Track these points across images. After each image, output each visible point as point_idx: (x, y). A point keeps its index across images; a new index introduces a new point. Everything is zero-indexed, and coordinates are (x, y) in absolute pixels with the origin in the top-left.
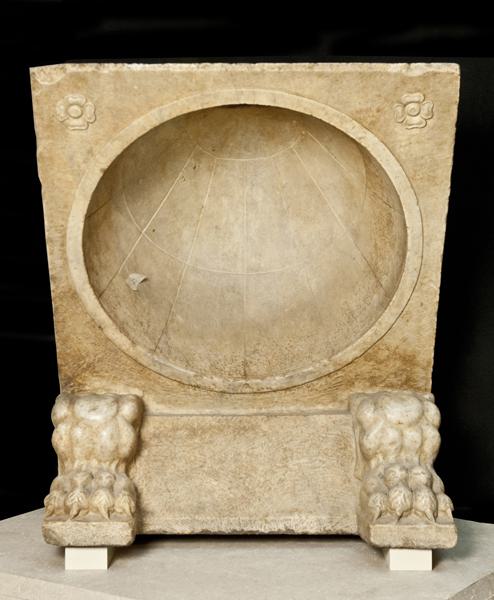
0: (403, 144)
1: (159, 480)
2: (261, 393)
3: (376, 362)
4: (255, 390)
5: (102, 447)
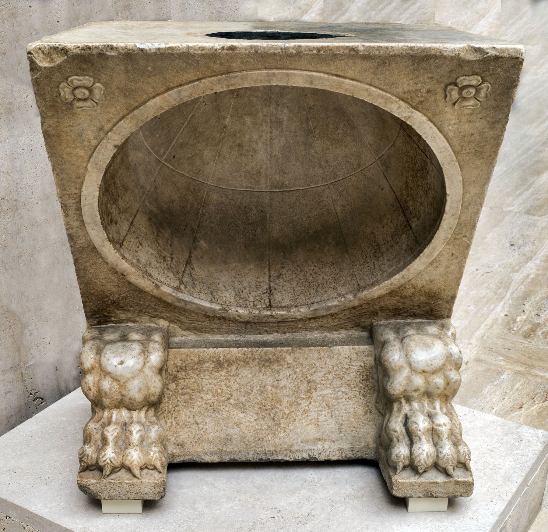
0: (452, 122)
1: (188, 413)
3: (401, 297)
4: (279, 320)
5: (130, 399)
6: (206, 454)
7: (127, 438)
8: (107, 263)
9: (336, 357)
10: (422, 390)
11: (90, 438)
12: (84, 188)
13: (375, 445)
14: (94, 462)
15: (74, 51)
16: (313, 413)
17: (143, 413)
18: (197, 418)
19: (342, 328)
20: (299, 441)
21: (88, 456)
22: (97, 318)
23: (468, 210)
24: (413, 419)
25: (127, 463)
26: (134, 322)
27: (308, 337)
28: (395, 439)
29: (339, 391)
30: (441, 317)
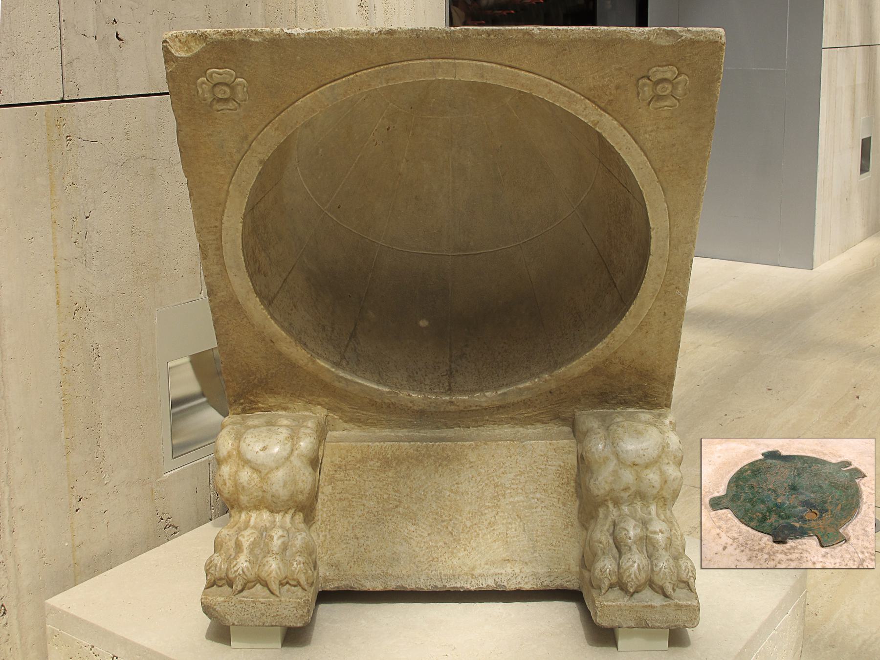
0: (649, 129)
4: (461, 408)
5: (272, 496)
7: (266, 545)
8: (253, 325)
9: (529, 454)
10: (633, 489)
11: (222, 546)
12: (225, 218)
13: (578, 569)
14: (223, 575)
15: (214, 37)
16: (501, 526)
17: (288, 517)
18: (357, 531)
19: (538, 421)
20: (483, 563)
21: (216, 565)
22: (242, 404)
23: (677, 249)
25: (263, 575)
26: (285, 409)
28: (600, 552)
30: (658, 406)
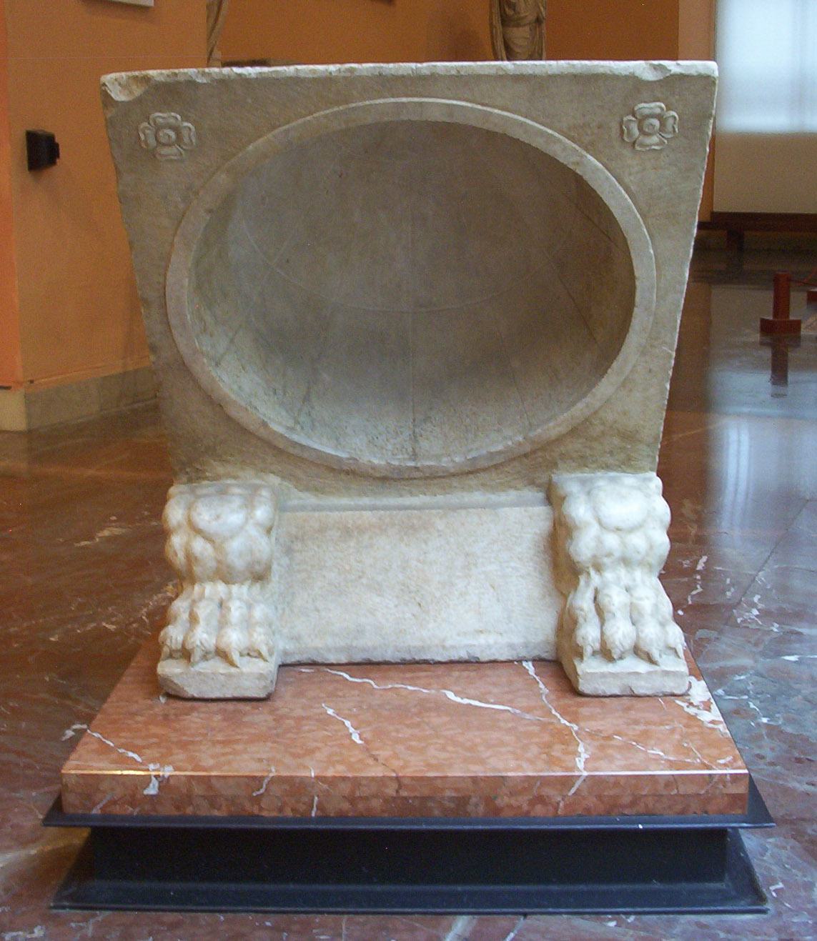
2: (435, 478)
6: (329, 650)
10: (617, 554)
12: (169, 274)
14: (179, 647)
24: (606, 591)
25: (222, 646)
27: (466, 499)
29: (507, 567)
